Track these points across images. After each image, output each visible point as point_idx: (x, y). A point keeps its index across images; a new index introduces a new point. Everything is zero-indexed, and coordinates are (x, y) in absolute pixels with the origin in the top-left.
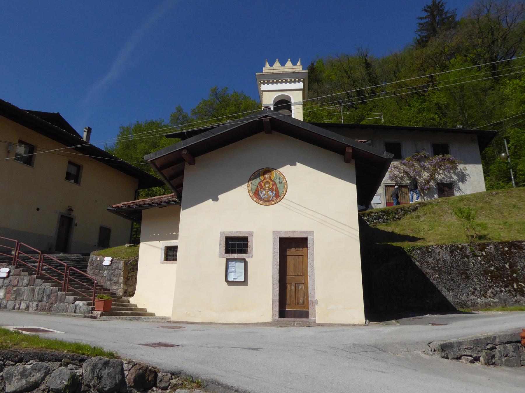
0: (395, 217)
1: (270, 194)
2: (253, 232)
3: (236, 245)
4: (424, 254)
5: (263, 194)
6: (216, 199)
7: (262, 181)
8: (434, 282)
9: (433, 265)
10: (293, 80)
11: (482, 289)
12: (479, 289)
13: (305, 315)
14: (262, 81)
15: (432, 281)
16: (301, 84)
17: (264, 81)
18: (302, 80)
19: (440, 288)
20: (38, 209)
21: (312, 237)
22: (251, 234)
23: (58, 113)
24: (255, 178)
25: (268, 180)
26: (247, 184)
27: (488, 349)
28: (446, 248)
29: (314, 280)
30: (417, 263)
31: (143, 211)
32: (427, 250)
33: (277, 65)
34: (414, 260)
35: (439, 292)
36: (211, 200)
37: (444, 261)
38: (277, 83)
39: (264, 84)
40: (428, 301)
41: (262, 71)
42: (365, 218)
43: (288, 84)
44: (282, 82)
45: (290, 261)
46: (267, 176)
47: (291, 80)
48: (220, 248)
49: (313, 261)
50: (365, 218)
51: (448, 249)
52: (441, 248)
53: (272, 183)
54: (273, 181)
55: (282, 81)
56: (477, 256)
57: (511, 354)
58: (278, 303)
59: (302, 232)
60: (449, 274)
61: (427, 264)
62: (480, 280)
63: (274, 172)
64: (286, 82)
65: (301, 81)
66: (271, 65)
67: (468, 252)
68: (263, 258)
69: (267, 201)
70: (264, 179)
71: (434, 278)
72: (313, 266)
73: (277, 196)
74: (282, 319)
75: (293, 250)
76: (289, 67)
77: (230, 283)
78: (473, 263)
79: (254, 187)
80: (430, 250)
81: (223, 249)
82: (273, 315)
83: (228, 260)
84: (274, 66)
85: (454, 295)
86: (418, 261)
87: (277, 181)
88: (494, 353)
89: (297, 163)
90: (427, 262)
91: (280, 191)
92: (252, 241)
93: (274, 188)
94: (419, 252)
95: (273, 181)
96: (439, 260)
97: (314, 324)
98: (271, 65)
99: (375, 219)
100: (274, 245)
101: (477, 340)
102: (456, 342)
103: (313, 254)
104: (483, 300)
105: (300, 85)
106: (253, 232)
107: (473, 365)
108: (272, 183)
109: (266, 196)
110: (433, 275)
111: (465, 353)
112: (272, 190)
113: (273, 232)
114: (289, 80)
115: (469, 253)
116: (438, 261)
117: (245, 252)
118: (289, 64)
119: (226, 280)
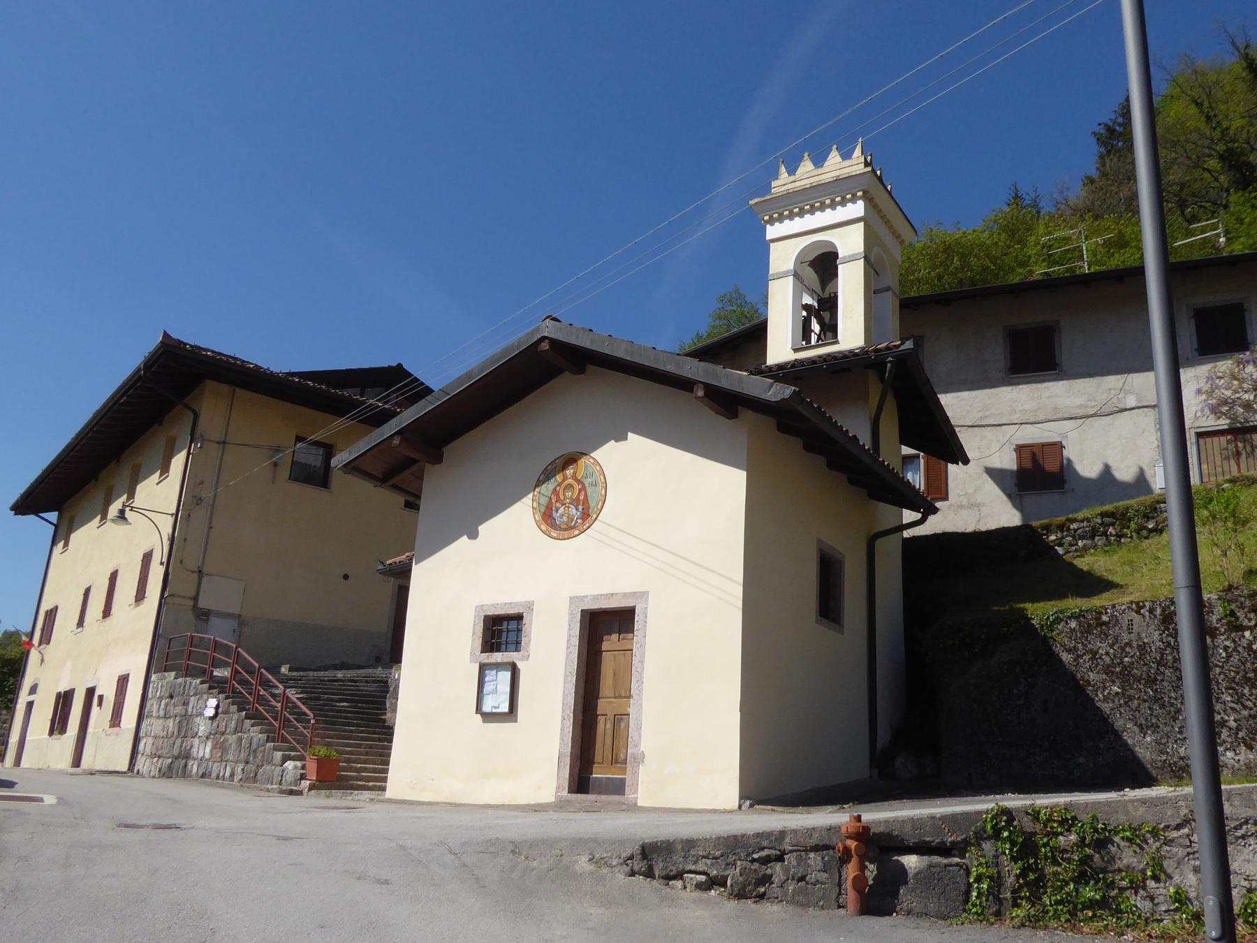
0: (1146, 528)
1: (570, 516)
2: (533, 603)
3: (501, 632)
4: (1087, 630)
5: (560, 513)
6: (473, 535)
7: (560, 485)
8: (1106, 707)
9: (1107, 659)
10: (838, 199)
11: (1244, 723)
12: (1233, 724)
13: (618, 787)
14: (766, 218)
15: (1098, 704)
16: (861, 203)
17: (771, 217)
18: (860, 194)
19: (1119, 724)
20: (346, 577)
21: (643, 605)
22: (530, 606)
23: (400, 365)
24: (548, 479)
25: (570, 481)
26: (530, 496)
27: (754, 860)
28: (1151, 611)
29: (641, 705)
30: (1066, 657)
31: (416, 570)
32: (1098, 619)
33: (806, 166)
34: (1057, 648)
35: (1117, 735)
36: (465, 538)
37: (1143, 648)
38: (801, 214)
39: (772, 225)
40: (1081, 760)
41: (768, 189)
42: (1053, 538)
43: (828, 211)
44: (812, 211)
45: (608, 664)
46: (569, 472)
47: (833, 200)
48: (473, 641)
49: (642, 662)
50: (1053, 538)
51: (1159, 611)
52: (1138, 612)
53: (577, 487)
54: (579, 482)
55: (812, 206)
56: (1242, 628)
57: (812, 877)
58: (568, 761)
59: (625, 595)
60: (1151, 681)
61: (1093, 658)
62: (1239, 699)
63: (583, 461)
64: (823, 208)
65: (860, 198)
66: (792, 172)
67: (1214, 618)
68: (550, 658)
69: (565, 530)
70: (564, 480)
71: (1107, 696)
72: (641, 675)
73: (586, 515)
74: (575, 796)
75: (615, 637)
76: (836, 166)
77: (489, 717)
78: (1226, 648)
79: (544, 501)
80: (1105, 618)
81: (479, 642)
82: (558, 788)
83: (483, 668)
84: (800, 171)
85: (1158, 743)
86: (1069, 651)
87: (586, 482)
88: (769, 871)
89: (630, 434)
90: (1094, 653)
91: (592, 504)
92: (531, 623)
93: (582, 497)
94: (1073, 624)
95: (579, 482)
96: (1129, 644)
97: (634, 808)
98: (792, 172)
99: (1082, 538)
100: (570, 629)
101: (735, 837)
102: (682, 841)
103: (643, 646)
104: (1242, 757)
105: (857, 209)
106: (533, 603)
107: (704, 895)
108: (577, 487)
109: (565, 519)
110: (1105, 688)
111: (693, 868)
112: (575, 502)
113: (571, 598)
114: (828, 202)
115: (1219, 620)
116: (1123, 649)
117: (517, 646)
118: (834, 158)
119: (479, 710)
